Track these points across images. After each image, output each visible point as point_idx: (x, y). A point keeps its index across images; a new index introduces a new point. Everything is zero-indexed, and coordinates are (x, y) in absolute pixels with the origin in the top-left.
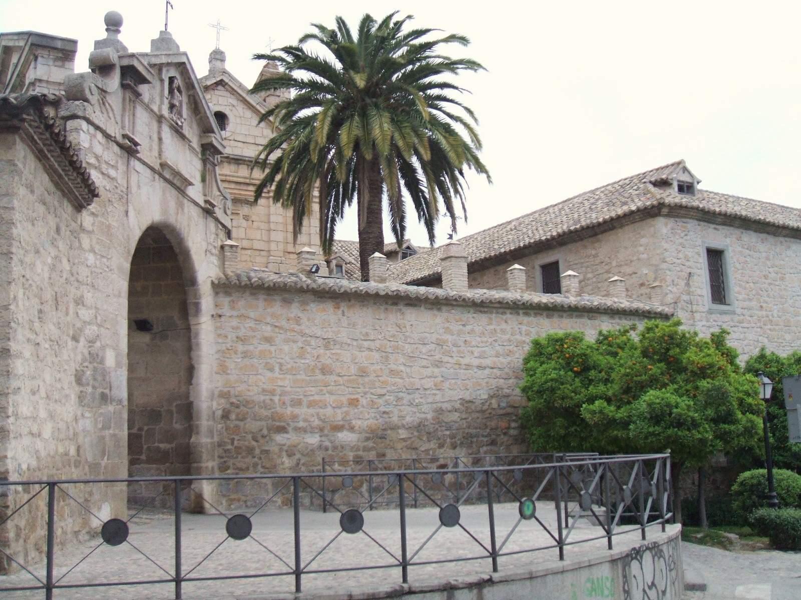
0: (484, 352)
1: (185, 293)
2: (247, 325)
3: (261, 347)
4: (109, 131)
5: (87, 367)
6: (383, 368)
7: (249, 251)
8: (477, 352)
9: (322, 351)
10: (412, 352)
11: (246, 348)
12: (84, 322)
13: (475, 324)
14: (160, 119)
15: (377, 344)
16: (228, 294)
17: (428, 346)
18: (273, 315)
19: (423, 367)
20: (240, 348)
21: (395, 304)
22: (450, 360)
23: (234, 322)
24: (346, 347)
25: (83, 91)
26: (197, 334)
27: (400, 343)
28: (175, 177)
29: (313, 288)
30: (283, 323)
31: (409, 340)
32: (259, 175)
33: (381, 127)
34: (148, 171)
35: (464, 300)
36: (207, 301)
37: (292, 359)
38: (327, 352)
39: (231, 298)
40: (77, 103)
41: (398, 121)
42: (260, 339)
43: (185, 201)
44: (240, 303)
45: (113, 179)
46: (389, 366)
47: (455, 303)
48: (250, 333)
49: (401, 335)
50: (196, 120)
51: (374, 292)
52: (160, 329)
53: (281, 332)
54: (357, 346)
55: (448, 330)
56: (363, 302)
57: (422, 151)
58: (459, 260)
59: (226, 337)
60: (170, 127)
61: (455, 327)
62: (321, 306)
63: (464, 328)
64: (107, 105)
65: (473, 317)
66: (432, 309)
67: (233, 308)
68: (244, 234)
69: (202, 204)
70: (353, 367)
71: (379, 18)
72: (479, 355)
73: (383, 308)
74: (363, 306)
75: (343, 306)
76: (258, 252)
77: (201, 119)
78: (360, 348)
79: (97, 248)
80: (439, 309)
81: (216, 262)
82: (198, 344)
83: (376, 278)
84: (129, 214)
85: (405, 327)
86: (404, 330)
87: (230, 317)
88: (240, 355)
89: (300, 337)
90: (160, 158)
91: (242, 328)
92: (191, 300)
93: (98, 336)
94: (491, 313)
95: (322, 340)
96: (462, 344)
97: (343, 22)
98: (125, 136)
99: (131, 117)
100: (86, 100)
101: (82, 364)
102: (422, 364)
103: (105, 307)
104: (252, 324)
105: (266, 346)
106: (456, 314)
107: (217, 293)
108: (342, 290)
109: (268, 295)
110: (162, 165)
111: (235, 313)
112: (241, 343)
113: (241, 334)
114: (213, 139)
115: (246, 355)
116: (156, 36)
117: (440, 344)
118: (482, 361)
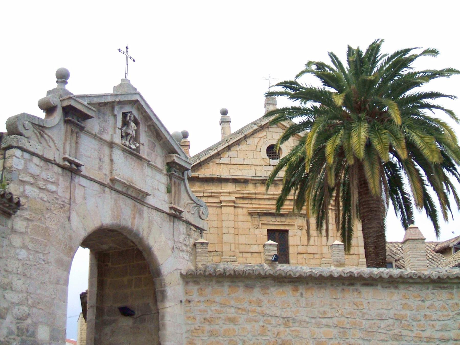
0: (446, 325)
1: (153, 284)
2: (213, 309)
3: (225, 327)
4: (46, 156)
5: (14, 339)
6: (342, 342)
7: (305, 255)
8: (438, 325)
9: (282, 329)
10: (370, 327)
11: (212, 328)
12: (12, 303)
13: (435, 300)
14: (111, 145)
15: (335, 320)
16: (196, 282)
17: (386, 321)
18: (237, 299)
19: (382, 340)
20: (207, 327)
21: (352, 284)
22: (410, 333)
23: (202, 307)
24: (305, 325)
25: (17, 127)
26: (163, 317)
27: (357, 319)
28: (128, 189)
29: (270, 274)
30: (246, 305)
31: (366, 317)
32: (276, 191)
33: (359, 136)
34: (97, 186)
35: (420, 277)
36: (174, 289)
37: (254, 336)
38: (287, 329)
39: (199, 287)
40: (12, 136)
41: (378, 129)
42: (225, 320)
43: (145, 209)
44: (207, 290)
45: (52, 192)
46: (347, 341)
47: (411, 281)
48: (217, 315)
49: (358, 312)
50: (160, 144)
51: (328, 275)
52: (140, 314)
53: (244, 313)
54: (316, 324)
55: (405, 306)
56: (320, 284)
57: (399, 152)
58: (417, 242)
59: (195, 319)
60: (123, 151)
61: (414, 303)
62: (280, 290)
63: (423, 304)
64: (45, 136)
65: (433, 293)
66: (389, 287)
67: (201, 294)
68: (299, 241)
69: (168, 210)
70: (311, 342)
71: (387, 50)
72: (440, 328)
73: (340, 289)
74: (321, 288)
75: (301, 289)
76: (312, 255)
77: (164, 142)
78: (319, 325)
79: (31, 246)
80: (396, 287)
81: (187, 257)
82: (164, 325)
83: (336, 263)
84: (71, 219)
85: (362, 305)
86: (361, 307)
87: (198, 302)
88: (206, 334)
89: (261, 317)
90: (111, 175)
91: (209, 311)
92: (158, 288)
93: (29, 314)
94: (453, 288)
95: (282, 320)
96: (423, 319)
97: (335, 56)
98: (65, 159)
99: (74, 145)
100: (20, 134)
101: (7, 336)
102: (381, 338)
103: (39, 292)
104: (218, 308)
105: (231, 326)
106: (413, 291)
107: (187, 283)
108: (298, 275)
109: (232, 282)
110: (111, 180)
111: (203, 299)
112: (208, 323)
113: (207, 316)
114: (175, 158)
115: (212, 334)
116: (118, 82)
117: (398, 319)
118: (443, 333)
